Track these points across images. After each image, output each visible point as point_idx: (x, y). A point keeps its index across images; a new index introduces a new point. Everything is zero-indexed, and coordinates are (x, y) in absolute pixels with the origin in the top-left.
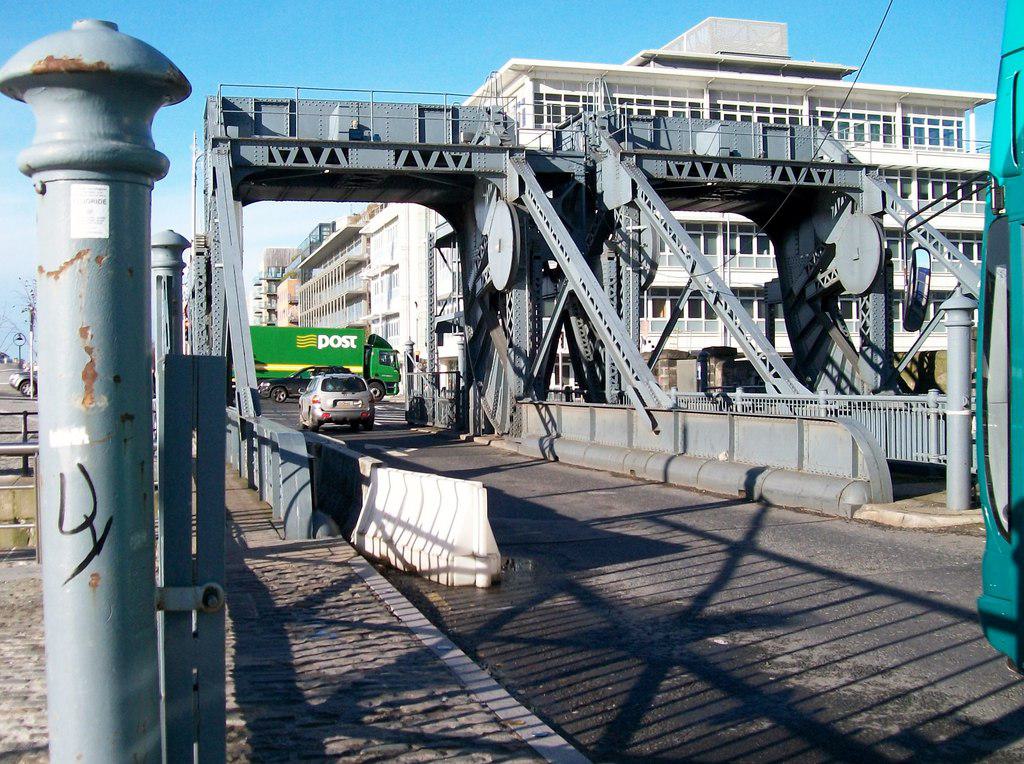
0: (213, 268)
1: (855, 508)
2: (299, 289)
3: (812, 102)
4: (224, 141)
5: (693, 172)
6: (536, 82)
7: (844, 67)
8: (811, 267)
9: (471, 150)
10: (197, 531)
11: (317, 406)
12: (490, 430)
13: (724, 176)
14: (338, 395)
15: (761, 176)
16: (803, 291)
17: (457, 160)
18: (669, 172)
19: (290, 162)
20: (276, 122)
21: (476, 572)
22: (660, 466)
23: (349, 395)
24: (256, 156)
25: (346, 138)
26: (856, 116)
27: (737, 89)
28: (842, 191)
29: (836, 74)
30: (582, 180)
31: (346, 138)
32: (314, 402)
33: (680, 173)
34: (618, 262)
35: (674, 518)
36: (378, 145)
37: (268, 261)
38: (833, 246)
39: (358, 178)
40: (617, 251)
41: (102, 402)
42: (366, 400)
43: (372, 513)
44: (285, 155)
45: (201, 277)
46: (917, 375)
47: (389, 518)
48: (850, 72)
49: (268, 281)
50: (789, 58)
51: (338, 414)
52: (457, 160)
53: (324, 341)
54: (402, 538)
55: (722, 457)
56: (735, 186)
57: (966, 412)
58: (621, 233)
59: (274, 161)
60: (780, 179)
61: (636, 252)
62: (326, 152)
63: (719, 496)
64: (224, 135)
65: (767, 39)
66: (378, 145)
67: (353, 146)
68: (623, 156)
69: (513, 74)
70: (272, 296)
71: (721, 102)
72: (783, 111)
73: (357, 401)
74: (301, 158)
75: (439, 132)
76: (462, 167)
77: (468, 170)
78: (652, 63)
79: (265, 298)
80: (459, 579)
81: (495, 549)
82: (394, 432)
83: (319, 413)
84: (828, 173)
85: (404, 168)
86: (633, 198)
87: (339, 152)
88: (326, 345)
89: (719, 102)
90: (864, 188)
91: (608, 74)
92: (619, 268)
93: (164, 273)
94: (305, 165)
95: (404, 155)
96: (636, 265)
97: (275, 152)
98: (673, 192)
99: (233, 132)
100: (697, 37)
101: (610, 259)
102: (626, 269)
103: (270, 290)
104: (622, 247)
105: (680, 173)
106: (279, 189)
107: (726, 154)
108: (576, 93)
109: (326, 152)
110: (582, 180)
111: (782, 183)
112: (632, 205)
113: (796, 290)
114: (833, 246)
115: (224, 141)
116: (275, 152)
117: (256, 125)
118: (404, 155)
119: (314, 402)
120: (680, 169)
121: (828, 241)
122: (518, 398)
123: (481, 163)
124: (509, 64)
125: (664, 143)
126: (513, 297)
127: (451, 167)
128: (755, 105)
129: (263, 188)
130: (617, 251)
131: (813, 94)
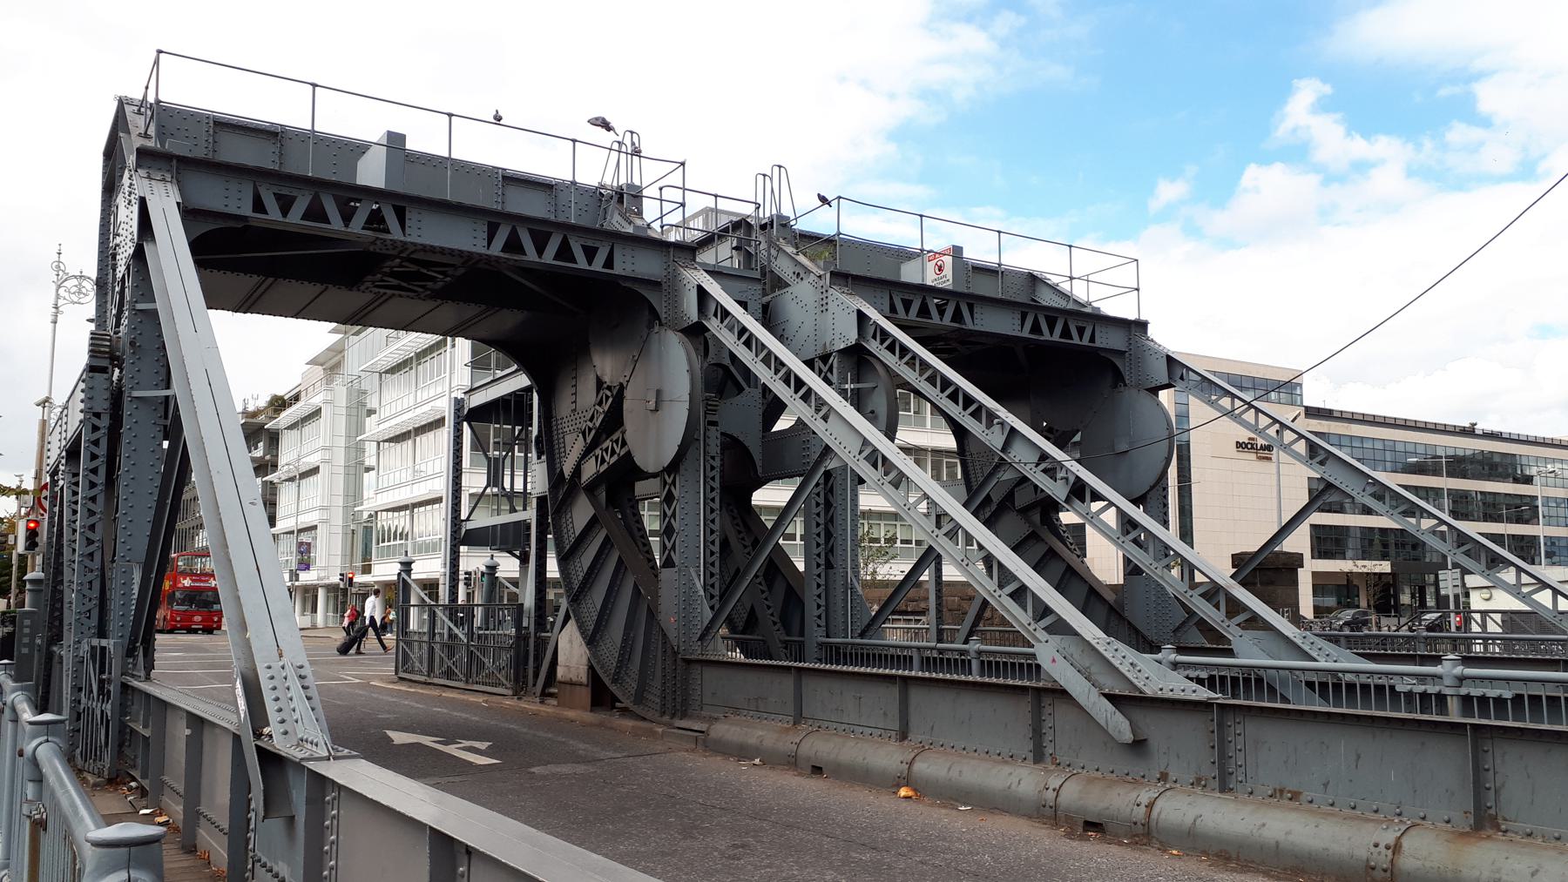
0: (126, 400)
8: (590, 430)
16: (577, 471)
33: (907, 311)
39: (413, 268)
44: (285, 205)
45: (98, 415)
52: (590, 253)
60: (557, 257)
76: (598, 265)
85: (502, 255)
94: (930, 321)
105: (907, 311)
113: (568, 469)
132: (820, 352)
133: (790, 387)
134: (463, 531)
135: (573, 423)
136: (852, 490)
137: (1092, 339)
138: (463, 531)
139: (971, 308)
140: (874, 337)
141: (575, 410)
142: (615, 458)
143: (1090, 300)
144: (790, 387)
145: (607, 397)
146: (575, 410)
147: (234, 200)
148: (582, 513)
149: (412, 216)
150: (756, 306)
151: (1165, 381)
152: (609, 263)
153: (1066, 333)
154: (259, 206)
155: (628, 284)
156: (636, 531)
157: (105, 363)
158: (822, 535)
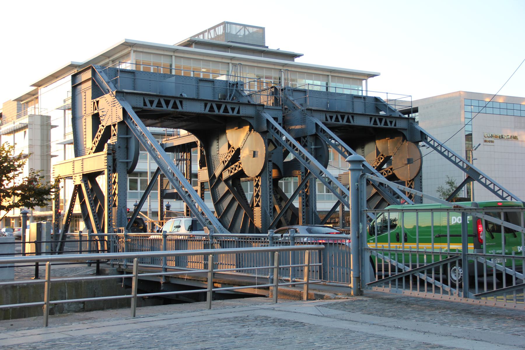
5: (159, 104)
8: (226, 161)
13: (350, 122)
15: (198, 108)
16: (221, 175)
35: (13, 337)
45: (110, 167)
53: (454, 219)
56: (183, 114)
59: (146, 106)
78: (194, 45)
88: (455, 222)
100: (215, 30)
111: (374, 126)
113: (217, 174)
132: (303, 135)
133: (291, 147)
134: (165, 193)
135: (216, 158)
136: (314, 181)
137: (395, 125)
138: (165, 193)
139: (353, 117)
140: (321, 132)
141: (218, 153)
142: (236, 171)
143: (396, 109)
144: (291, 147)
145: (233, 151)
146: (218, 153)
147: (140, 104)
148: (223, 188)
149: (184, 103)
150: (280, 120)
151: (420, 140)
152: (238, 112)
153: (386, 124)
154: (145, 104)
155: (244, 118)
156: (242, 195)
157: (111, 152)
158: (305, 196)
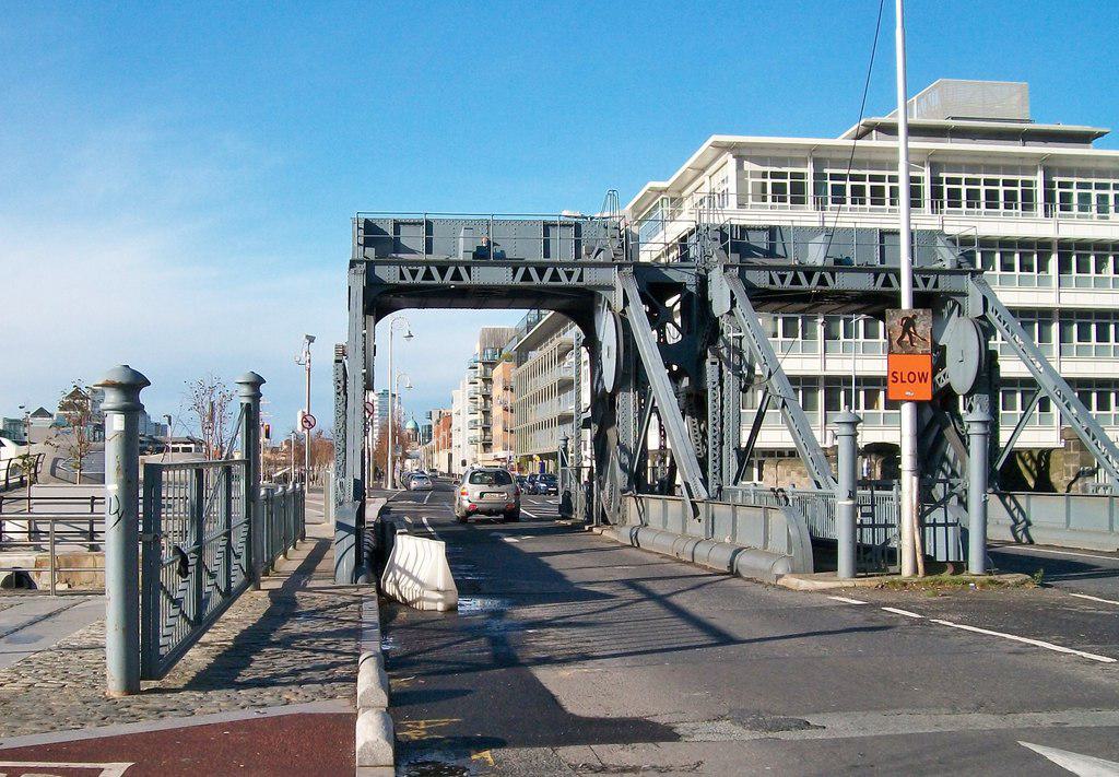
1: (779, 577)
2: (514, 372)
3: (1048, 173)
4: (361, 262)
6: (740, 159)
7: (1094, 130)
9: (583, 265)
10: (144, 519)
11: (465, 497)
12: (606, 522)
14: (485, 488)
17: (569, 275)
18: (772, 282)
19: (419, 280)
20: (413, 239)
21: (436, 601)
22: (727, 555)
23: (496, 488)
24: (388, 274)
25: (470, 257)
26: (1098, 186)
27: (960, 160)
28: (948, 295)
29: (1084, 138)
30: (693, 289)
31: (470, 257)
32: (463, 494)
33: (783, 282)
34: (721, 367)
36: (501, 260)
37: (483, 341)
38: (945, 346)
40: (719, 356)
41: (122, 477)
42: (512, 493)
43: (393, 565)
44: (414, 274)
46: (1036, 472)
47: (399, 568)
48: (1101, 135)
49: (484, 364)
50: (1030, 121)
51: (484, 506)
52: (569, 275)
54: (406, 583)
55: (727, 540)
57: (850, 502)
58: (724, 340)
61: (737, 357)
62: (451, 270)
63: (705, 567)
64: (361, 257)
65: (1006, 101)
66: (501, 260)
67: (475, 264)
68: (726, 268)
69: (716, 151)
70: (488, 380)
71: (944, 175)
72: (1014, 183)
73: (503, 493)
74: (428, 275)
75: (562, 250)
77: (579, 284)
78: (874, 132)
79: (480, 383)
80: (427, 606)
81: (453, 586)
82: (545, 523)
83: (467, 504)
84: (932, 278)
85: (521, 283)
86: (732, 307)
87: (462, 270)
89: (941, 175)
90: (970, 292)
91: (818, 148)
92: (721, 371)
93: (245, 401)
94: (433, 282)
95: (521, 271)
96: (736, 370)
97: (406, 271)
98: (761, 298)
99: (371, 253)
101: (713, 363)
102: (727, 372)
103: (485, 374)
104: (724, 352)
105: (783, 282)
106: (418, 300)
107: (831, 262)
108: (784, 170)
109: (451, 270)
110: (693, 289)
112: (730, 313)
114: (945, 346)
115: (361, 262)
116: (406, 271)
117: (397, 246)
118: (521, 271)
119: (463, 494)
120: (783, 278)
121: (941, 344)
122: (623, 491)
123: (591, 277)
124: (714, 138)
125: (779, 250)
126: (620, 399)
127: (564, 281)
128: (982, 177)
129: (402, 300)
130: (719, 356)
131: (1049, 164)
